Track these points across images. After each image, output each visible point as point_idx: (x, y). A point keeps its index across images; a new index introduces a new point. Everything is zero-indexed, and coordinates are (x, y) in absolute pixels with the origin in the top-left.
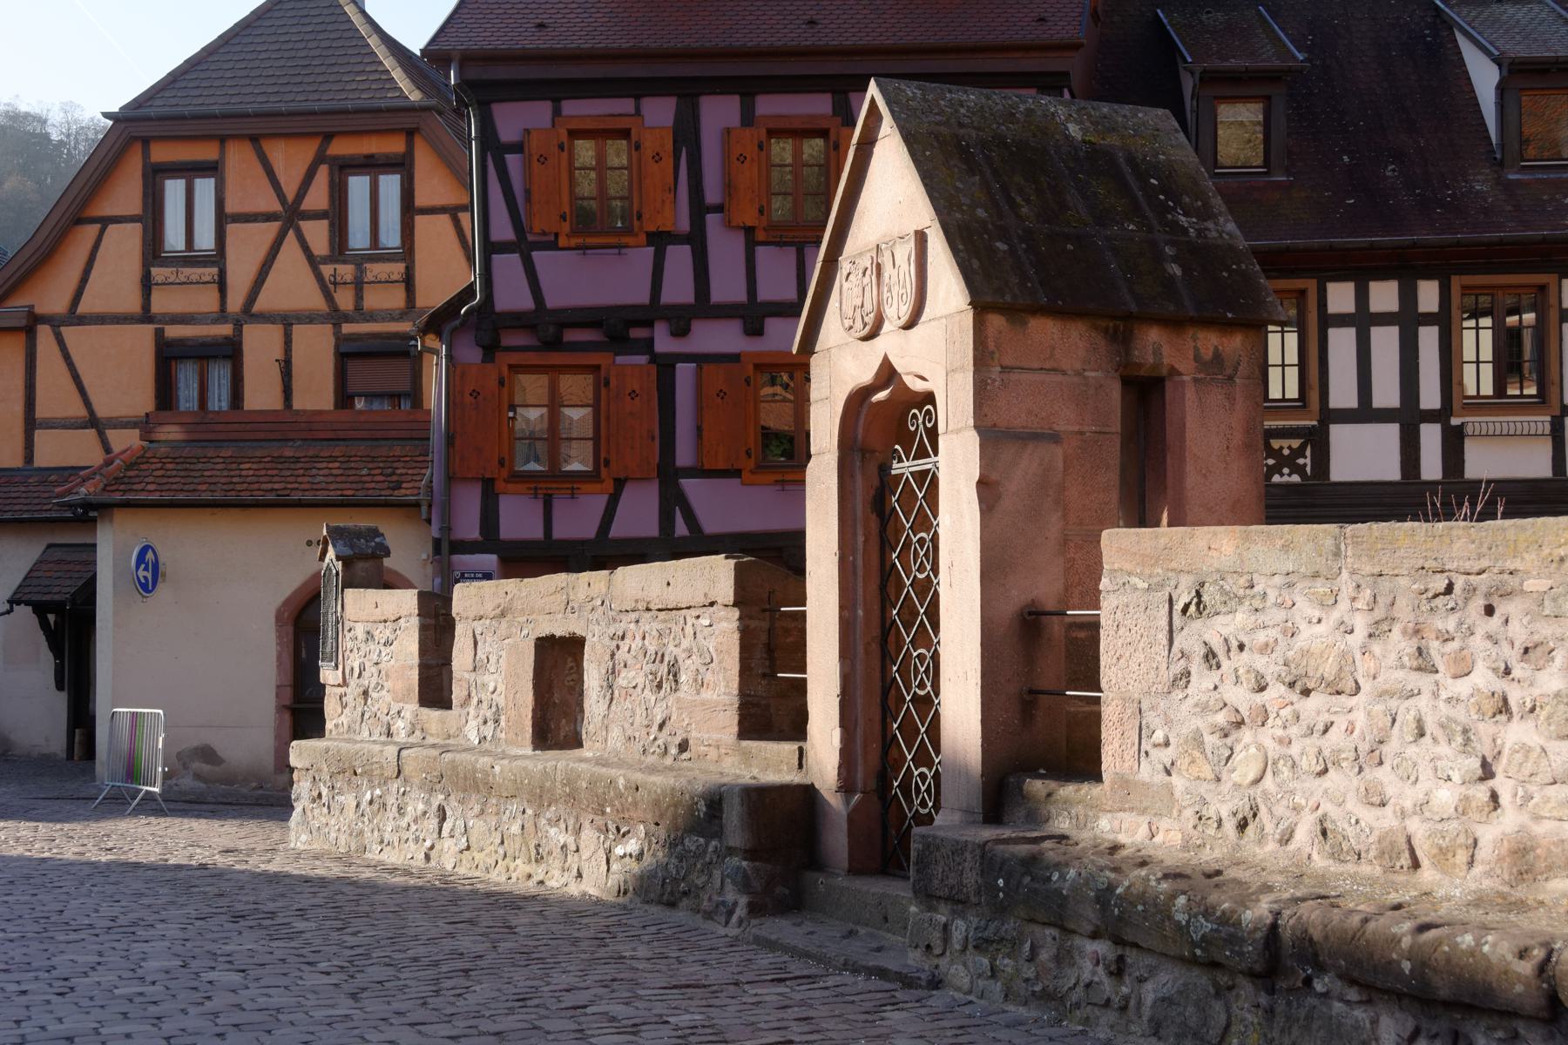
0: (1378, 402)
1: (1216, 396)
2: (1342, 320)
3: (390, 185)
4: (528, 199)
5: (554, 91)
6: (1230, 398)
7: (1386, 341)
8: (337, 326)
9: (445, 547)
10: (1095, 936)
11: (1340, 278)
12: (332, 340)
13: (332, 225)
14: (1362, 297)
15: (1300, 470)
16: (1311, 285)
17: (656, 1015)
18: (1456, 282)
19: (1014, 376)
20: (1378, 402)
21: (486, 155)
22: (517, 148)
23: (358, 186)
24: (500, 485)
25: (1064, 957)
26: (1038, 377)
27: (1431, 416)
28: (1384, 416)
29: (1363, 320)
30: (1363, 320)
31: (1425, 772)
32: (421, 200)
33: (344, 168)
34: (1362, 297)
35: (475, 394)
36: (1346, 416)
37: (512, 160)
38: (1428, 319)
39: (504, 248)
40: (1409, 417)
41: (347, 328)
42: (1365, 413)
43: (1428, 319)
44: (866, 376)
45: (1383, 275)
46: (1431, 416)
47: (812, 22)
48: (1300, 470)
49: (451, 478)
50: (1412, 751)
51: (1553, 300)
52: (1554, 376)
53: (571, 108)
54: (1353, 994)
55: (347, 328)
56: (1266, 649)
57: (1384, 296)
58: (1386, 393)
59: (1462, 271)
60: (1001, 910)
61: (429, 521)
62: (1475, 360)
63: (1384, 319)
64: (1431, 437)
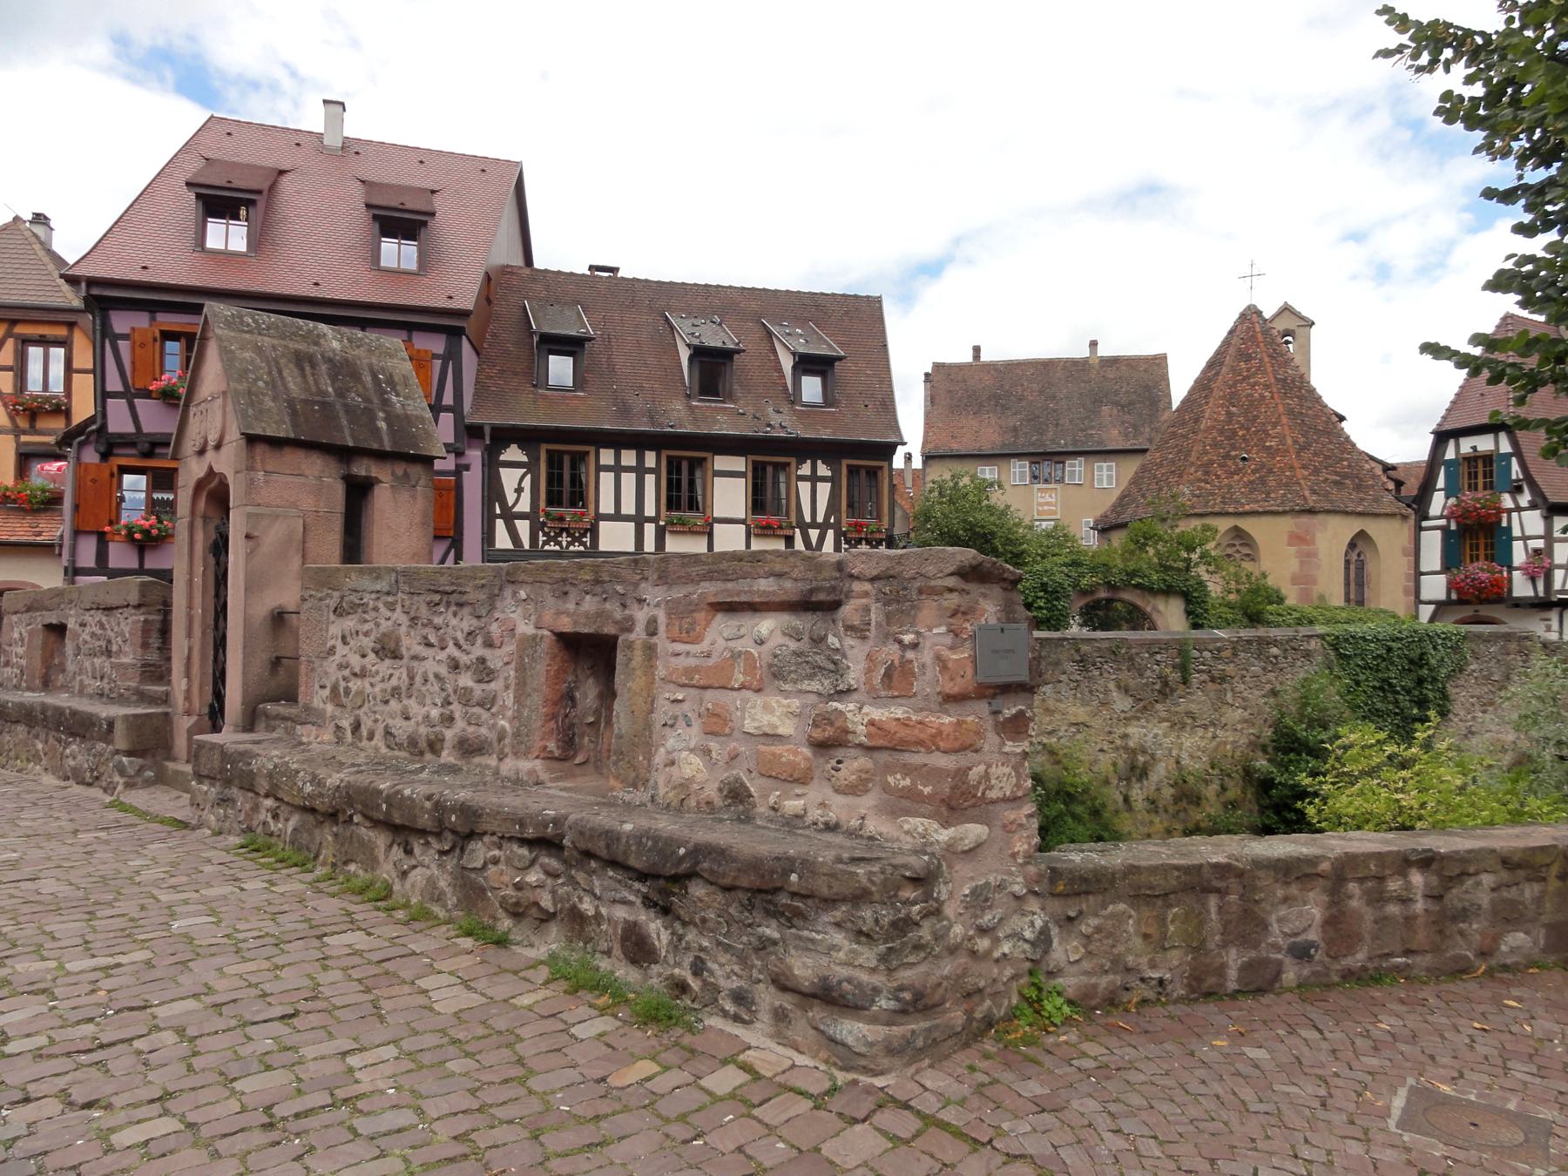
0: (624, 511)
1: (405, 496)
2: (607, 469)
3: (58, 353)
4: (134, 370)
5: (152, 307)
6: (414, 497)
7: (628, 480)
8: (17, 436)
9: (70, 570)
10: (267, 796)
11: (607, 447)
12: (14, 445)
13: (15, 375)
14: (618, 458)
15: (584, 544)
16: (592, 449)
17: (41, 848)
18: (664, 454)
19: (274, 477)
20: (624, 511)
21: (794, 390)
22: (125, 337)
23: (35, 353)
24: (108, 537)
25: (256, 808)
26: (290, 479)
27: (650, 520)
28: (627, 518)
29: (618, 469)
30: (618, 469)
31: (428, 701)
32: (76, 365)
33: (27, 341)
34: (618, 458)
35: (94, 481)
36: (608, 518)
37: (124, 346)
38: (650, 471)
39: (115, 395)
40: (639, 520)
41: (23, 438)
42: (617, 516)
43: (650, 471)
44: (202, 474)
45: (628, 447)
46: (650, 520)
47: (316, 284)
48: (584, 544)
49: (77, 533)
50: (424, 689)
51: (709, 466)
52: (709, 503)
53: (161, 317)
54: (368, 824)
55: (23, 438)
56: (366, 634)
57: (628, 457)
58: (629, 507)
59: (667, 449)
60: (228, 783)
61: (60, 555)
62: (1527, 534)
63: (628, 469)
64: (649, 529)
